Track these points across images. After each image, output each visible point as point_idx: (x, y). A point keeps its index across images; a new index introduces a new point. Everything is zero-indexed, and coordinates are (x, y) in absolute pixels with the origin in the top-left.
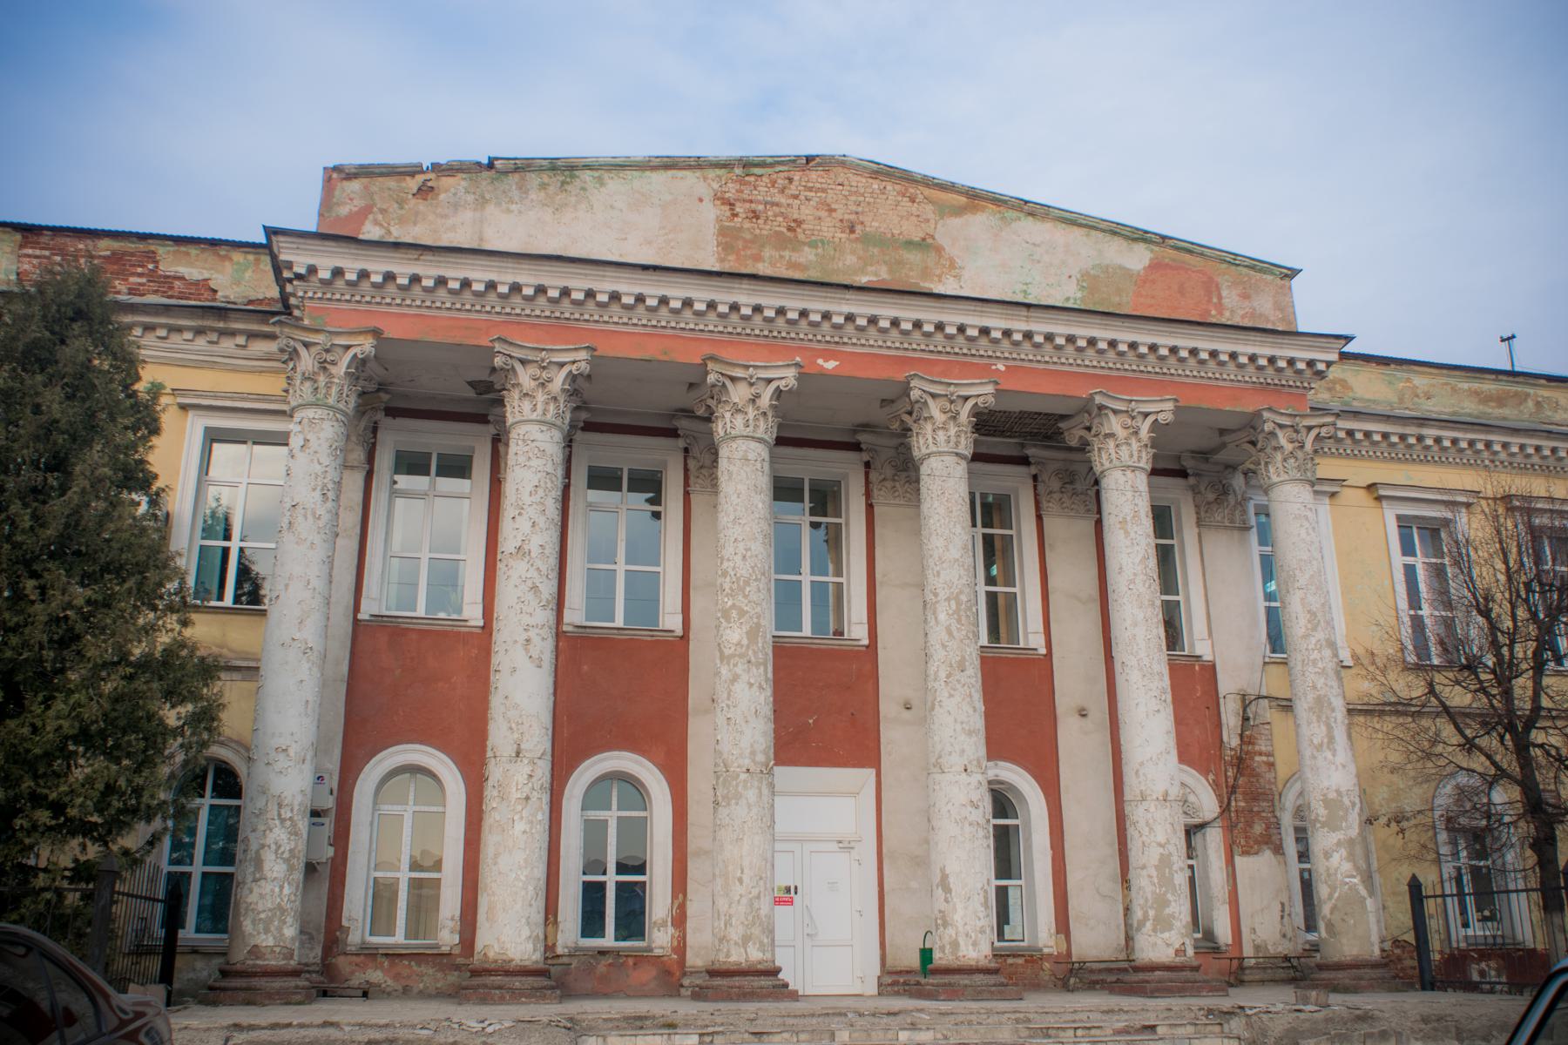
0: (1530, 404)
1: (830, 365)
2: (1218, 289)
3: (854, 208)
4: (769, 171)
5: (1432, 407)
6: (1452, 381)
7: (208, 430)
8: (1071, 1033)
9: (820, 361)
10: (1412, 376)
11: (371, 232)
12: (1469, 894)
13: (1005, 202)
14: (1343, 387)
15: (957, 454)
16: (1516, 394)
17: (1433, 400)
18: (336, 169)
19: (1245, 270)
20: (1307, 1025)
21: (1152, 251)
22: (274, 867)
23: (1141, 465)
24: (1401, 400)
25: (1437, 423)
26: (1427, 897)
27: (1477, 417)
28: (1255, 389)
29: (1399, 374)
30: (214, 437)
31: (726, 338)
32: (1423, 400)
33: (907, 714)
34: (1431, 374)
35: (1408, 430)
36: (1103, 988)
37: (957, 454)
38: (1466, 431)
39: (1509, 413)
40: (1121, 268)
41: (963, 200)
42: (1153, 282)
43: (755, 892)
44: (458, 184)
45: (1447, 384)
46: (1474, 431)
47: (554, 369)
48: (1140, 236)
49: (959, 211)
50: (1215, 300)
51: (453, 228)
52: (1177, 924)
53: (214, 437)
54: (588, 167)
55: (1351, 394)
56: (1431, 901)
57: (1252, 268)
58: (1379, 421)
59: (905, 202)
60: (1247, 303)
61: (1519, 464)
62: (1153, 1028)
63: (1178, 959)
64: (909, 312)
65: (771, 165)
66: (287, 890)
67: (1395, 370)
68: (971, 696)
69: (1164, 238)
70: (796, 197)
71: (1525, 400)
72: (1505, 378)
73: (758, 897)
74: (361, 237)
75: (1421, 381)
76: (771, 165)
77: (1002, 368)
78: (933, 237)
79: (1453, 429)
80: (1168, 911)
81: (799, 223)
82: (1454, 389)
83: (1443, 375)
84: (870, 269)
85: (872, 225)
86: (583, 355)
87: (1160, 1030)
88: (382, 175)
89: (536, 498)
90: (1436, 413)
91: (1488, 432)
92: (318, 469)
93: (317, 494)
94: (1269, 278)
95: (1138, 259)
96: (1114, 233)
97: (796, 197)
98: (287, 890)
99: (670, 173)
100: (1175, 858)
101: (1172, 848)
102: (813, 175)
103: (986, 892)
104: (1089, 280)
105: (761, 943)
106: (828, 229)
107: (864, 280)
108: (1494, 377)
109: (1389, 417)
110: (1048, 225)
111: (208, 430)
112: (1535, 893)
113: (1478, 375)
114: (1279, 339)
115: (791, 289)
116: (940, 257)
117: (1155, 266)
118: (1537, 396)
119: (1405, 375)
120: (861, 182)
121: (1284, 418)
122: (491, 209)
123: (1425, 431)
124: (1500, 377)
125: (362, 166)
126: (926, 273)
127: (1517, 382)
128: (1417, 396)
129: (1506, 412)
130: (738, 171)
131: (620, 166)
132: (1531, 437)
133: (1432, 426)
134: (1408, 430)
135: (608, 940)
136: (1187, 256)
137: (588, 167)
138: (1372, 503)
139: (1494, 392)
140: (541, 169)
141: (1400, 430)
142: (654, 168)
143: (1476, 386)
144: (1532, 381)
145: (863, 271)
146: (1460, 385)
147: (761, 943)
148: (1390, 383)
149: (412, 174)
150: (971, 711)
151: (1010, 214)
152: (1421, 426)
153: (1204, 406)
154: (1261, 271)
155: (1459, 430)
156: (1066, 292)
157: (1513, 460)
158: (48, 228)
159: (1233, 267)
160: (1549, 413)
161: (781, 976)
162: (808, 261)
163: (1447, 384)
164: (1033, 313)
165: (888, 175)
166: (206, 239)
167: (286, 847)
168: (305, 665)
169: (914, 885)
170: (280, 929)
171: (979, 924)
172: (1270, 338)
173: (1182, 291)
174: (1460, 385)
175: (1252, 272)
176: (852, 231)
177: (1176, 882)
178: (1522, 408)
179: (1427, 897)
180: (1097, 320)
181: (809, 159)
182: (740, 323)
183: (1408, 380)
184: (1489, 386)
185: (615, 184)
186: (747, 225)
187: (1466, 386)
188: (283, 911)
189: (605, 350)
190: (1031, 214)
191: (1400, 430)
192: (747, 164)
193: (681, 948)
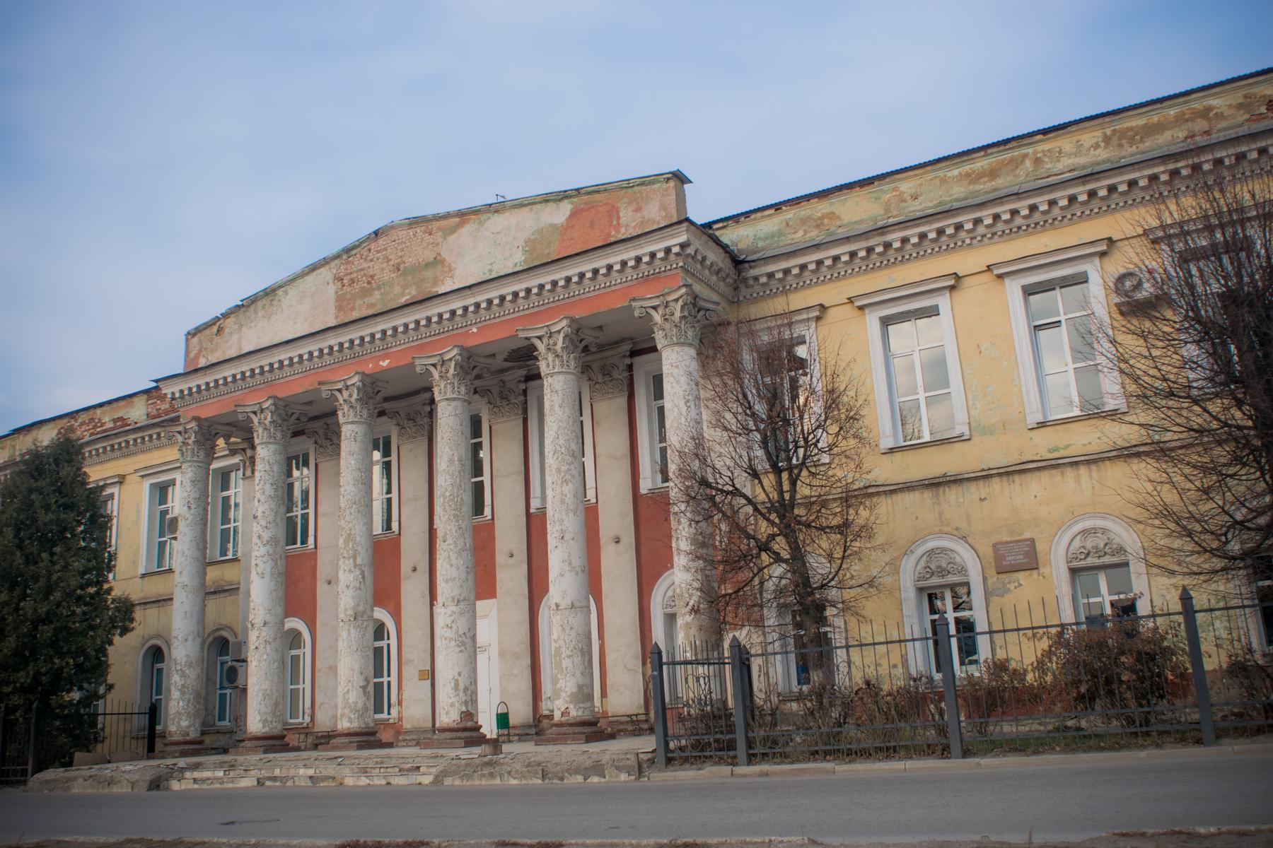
0: (1028, 163)
1: (385, 364)
2: (618, 212)
3: (399, 254)
4: (359, 249)
5: (916, 208)
6: (940, 174)
7: (881, 319)
8: (377, 771)
9: (381, 363)
10: (898, 184)
11: (202, 362)
12: (953, 636)
13: (479, 210)
14: (831, 219)
15: (447, 399)
16: (1012, 160)
17: (921, 199)
18: (188, 333)
19: (639, 188)
20: (453, 768)
21: (572, 203)
22: (175, 694)
23: (556, 370)
24: (887, 210)
25: (896, 227)
26: (836, 648)
27: (965, 199)
28: (640, 283)
29: (885, 188)
30: (886, 322)
31: (337, 365)
32: (910, 202)
33: (511, 561)
34: (916, 175)
35: (871, 243)
36: (625, 734)
37: (447, 399)
38: (930, 223)
39: (1003, 183)
40: (551, 225)
41: (457, 220)
42: (573, 227)
43: (346, 689)
44: (231, 321)
45: (936, 178)
46: (938, 220)
47: (556, 335)
48: (563, 196)
49: (454, 230)
50: (615, 223)
51: (230, 348)
52: (563, 694)
53: (886, 322)
54: (280, 287)
55: (838, 223)
56: (838, 651)
57: (642, 184)
58: (843, 244)
59: (427, 237)
60: (639, 215)
61: (1003, 232)
62: (418, 768)
63: (563, 719)
64: (433, 310)
65: (359, 245)
66: (181, 704)
67: (879, 185)
68: (449, 557)
69: (577, 190)
70: (372, 260)
71: (1022, 162)
72: (994, 150)
73: (348, 692)
74: (199, 366)
75: (906, 186)
76: (359, 245)
77: (475, 330)
78: (440, 254)
79: (1065, 188)
80: (558, 686)
81: (372, 277)
82: (943, 181)
83: (929, 172)
84: (407, 291)
85: (410, 261)
86: (683, 290)
87: (422, 769)
88: (204, 329)
89: (260, 486)
90: (920, 210)
91: (953, 216)
92: (186, 494)
93: (186, 508)
94: (657, 186)
95: (560, 214)
96: (547, 201)
97: (372, 260)
98: (181, 704)
99: (315, 273)
100: (563, 650)
101: (561, 643)
102: (380, 241)
103: (457, 681)
104: (531, 246)
105: (350, 718)
106: (387, 275)
107: (403, 300)
108: (983, 153)
109: (847, 238)
110: (507, 214)
111: (881, 319)
112: (838, 645)
113: (965, 158)
114: (636, 242)
115: (351, 328)
116: (443, 266)
117: (574, 214)
118: (1035, 152)
119: (892, 185)
120: (403, 234)
121: (653, 300)
122: (244, 329)
123: (889, 238)
124: (989, 151)
125: (196, 328)
126: (436, 282)
127: (1010, 149)
128: (905, 201)
129: (1000, 182)
130: (345, 257)
131: (292, 280)
132: (1002, 203)
133: (893, 231)
134: (871, 243)
135: (385, 716)
136: (597, 195)
137: (280, 287)
138: (858, 312)
139: (986, 167)
140: (262, 297)
141: (864, 244)
142: (307, 274)
143: (967, 168)
144: (1026, 141)
145: (403, 294)
146: (949, 174)
147: (350, 718)
148: (876, 199)
149: (215, 324)
150: (448, 567)
151: (486, 216)
152: (883, 234)
153: (602, 310)
154: (650, 183)
155: (923, 224)
156: (516, 260)
157: (994, 230)
158: (742, 214)
159: (630, 190)
160: (1049, 166)
161: (482, 730)
162: (377, 301)
163: (936, 178)
164: (474, 290)
165: (416, 223)
166: (855, 182)
167: (180, 684)
168: (184, 594)
169: (515, 671)
170: (178, 723)
171: (451, 701)
172: (630, 244)
173: (592, 226)
174: (949, 174)
175: (644, 188)
176: (399, 270)
177: (564, 666)
178: (1018, 171)
179: (836, 648)
180: (512, 279)
181: (376, 233)
182: (291, 369)
183: (895, 189)
184: (981, 164)
185: (293, 291)
186: (349, 289)
187: (956, 172)
188: (180, 714)
189: (579, 314)
190: (496, 211)
191: (864, 244)
192: (347, 251)
193: (400, 719)
